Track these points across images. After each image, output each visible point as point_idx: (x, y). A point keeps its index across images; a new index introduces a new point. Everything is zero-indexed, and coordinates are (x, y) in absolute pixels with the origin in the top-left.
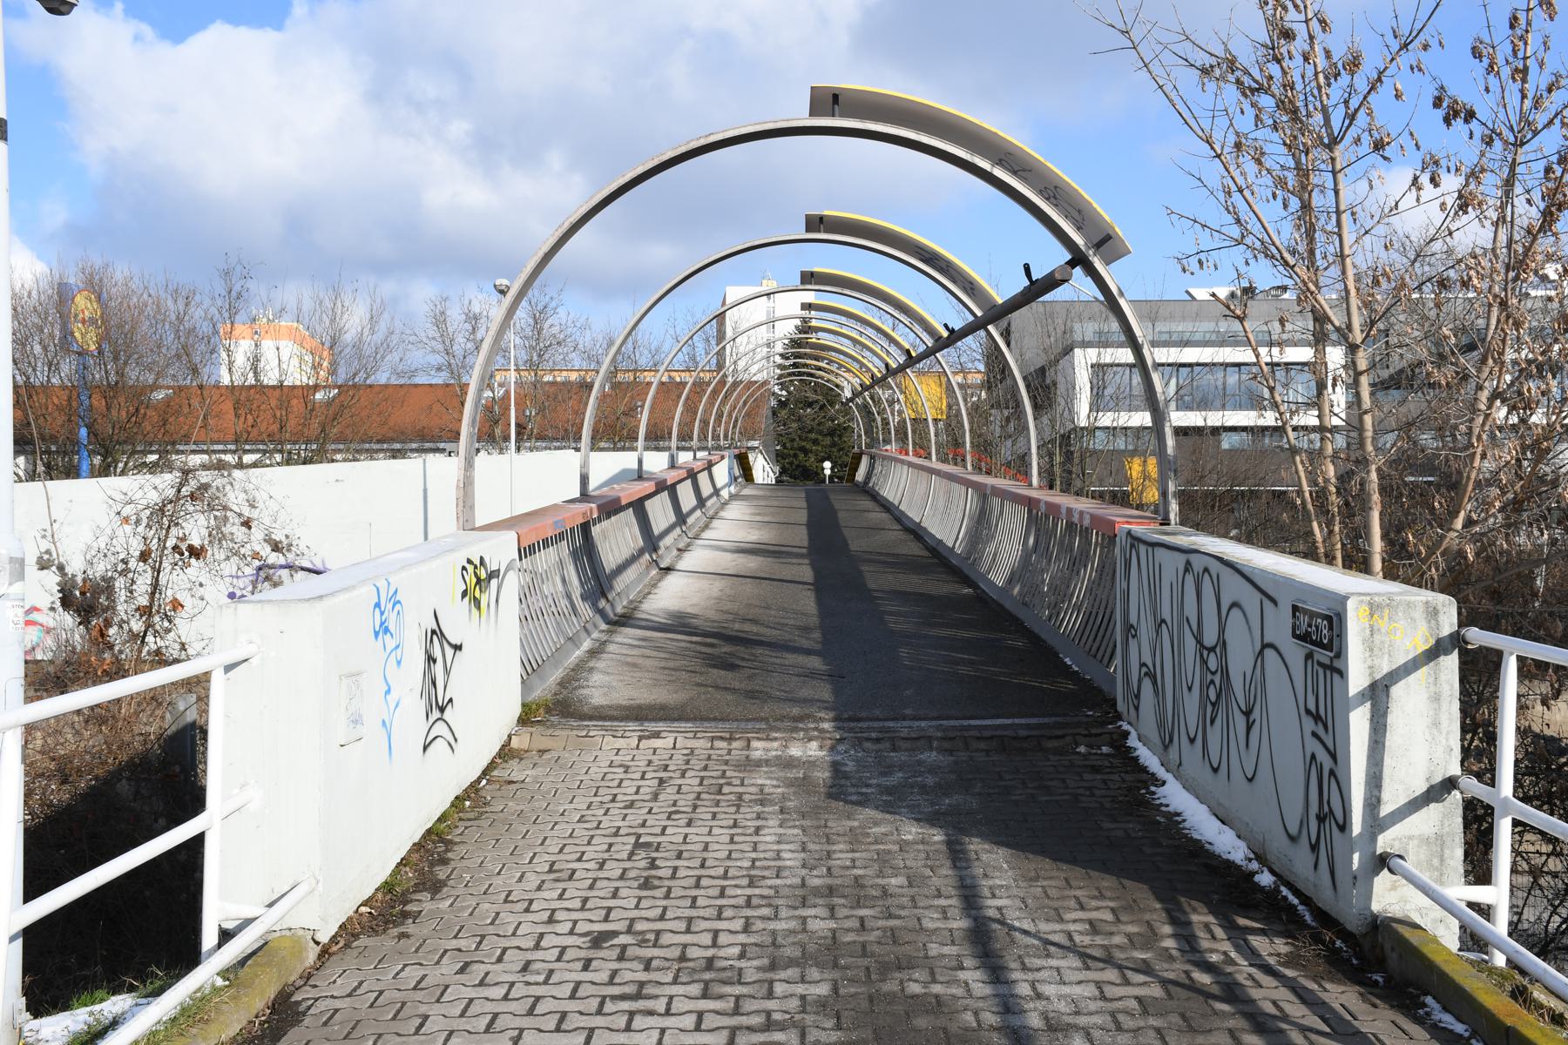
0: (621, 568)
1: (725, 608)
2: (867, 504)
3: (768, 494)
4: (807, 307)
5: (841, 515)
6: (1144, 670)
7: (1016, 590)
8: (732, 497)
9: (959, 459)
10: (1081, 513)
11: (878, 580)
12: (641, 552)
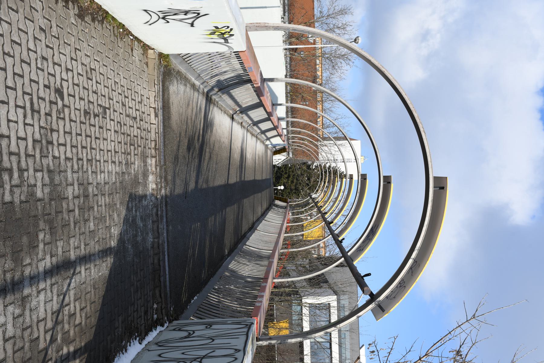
1: (216, 144)
2: (265, 206)
3: (268, 162)
4: (351, 177)
5: (260, 194)
6: (192, 332)
7: (227, 274)
8: (266, 146)
11: (230, 212)
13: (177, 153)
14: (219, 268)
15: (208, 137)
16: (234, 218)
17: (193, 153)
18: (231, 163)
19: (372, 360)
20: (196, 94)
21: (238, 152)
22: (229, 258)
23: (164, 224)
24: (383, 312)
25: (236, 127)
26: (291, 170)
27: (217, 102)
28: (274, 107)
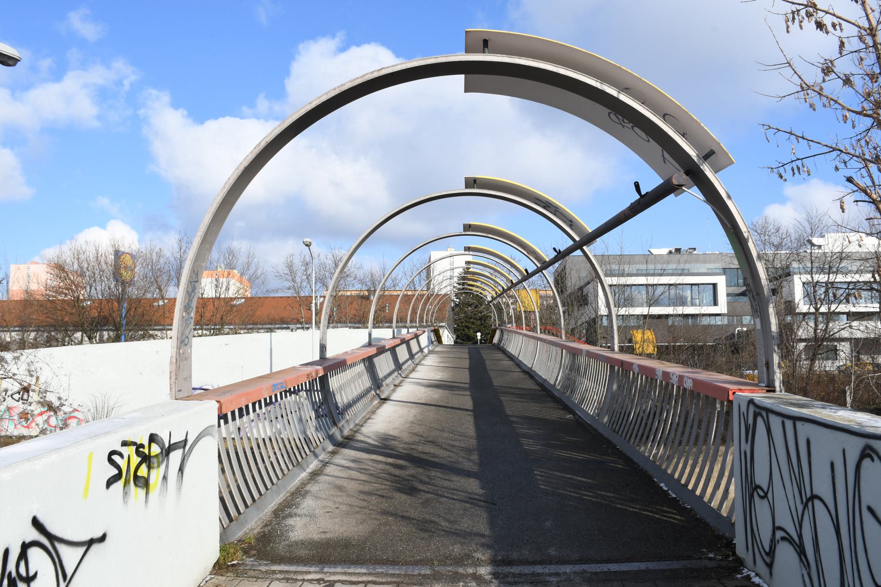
0: (386, 377)
1: (415, 431)
2: (500, 356)
3: (449, 350)
4: (468, 263)
5: (487, 362)
6: (779, 534)
7: (606, 419)
8: (430, 352)
9: (534, 329)
10: (681, 378)
11: (513, 407)
12: (368, 391)
13: (414, 525)
14: (596, 430)
15: (401, 446)
16: (520, 402)
17: (421, 481)
18: (444, 405)
19: (811, 173)
20: (330, 469)
21: (430, 392)
22: (578, 413)
23: (547, 571)
24: (714, 153)
25: (399, 394)
26: (460, 325)
27: (356, 425)
28: (373, 344)
